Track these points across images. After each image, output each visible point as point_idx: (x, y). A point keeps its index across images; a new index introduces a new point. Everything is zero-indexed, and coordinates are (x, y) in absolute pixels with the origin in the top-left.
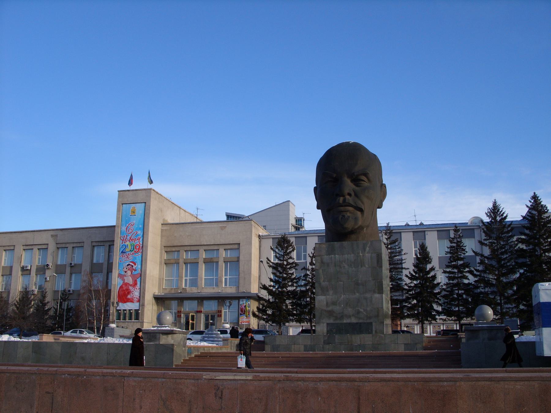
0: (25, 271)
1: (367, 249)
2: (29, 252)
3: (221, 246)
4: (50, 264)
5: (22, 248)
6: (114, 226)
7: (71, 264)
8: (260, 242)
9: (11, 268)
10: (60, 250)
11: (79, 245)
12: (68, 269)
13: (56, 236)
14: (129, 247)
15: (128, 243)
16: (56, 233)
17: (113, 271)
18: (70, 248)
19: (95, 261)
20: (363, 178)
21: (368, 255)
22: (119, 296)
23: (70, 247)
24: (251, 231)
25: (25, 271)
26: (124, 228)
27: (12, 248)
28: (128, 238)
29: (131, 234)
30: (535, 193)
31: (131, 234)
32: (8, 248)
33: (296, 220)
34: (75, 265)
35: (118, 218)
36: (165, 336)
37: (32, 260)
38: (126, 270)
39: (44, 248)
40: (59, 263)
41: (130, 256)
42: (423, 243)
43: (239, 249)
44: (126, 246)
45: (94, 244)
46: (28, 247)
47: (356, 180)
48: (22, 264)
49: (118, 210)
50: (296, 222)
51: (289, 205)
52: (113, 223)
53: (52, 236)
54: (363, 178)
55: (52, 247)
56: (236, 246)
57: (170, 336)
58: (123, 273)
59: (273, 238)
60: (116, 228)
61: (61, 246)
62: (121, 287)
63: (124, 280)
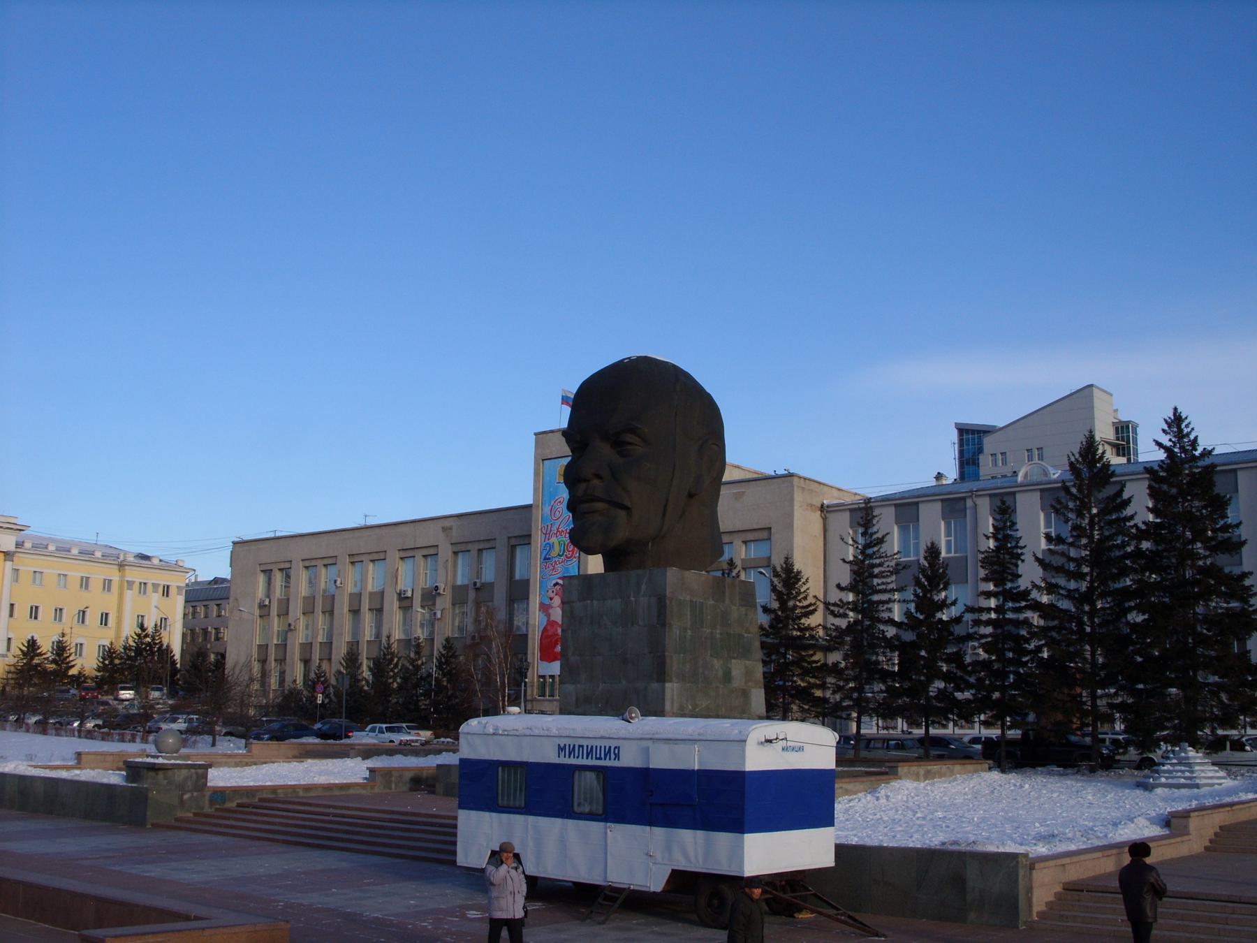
0: (405, 601)
1: (644, 587)
2: (410, 562)
3: (736, 535)
4: (442, 586)
5: (398, 555)
6: (529, 506)
7: (475, 584)
8: (825, 519)
9: (382, 593)
10: (460, 555)
11: (487, 545)
12: (472, 594)
13: (451, 528)
14: (557, 548)
15: (554, 540)
16: (445, 523)
17: (531, 596)
18: (474, 553)
19: (517, 577)
20: (629, 438)
21: (644, 600)
22: (542, 649)
23: (474, 548)
24: (792, 500)
25: (405, 601)
26: (547, 510)
27: (432, 551)
28: (555, 528)
29: (558, 522)
30: (1176, 409)
31: (558, 522)
32: (375, 557)
33: (1117, 429)
34: (483, 585)
35: (536, 490)
36: (152, 774)
37: (410, 577)
38: (552, 595)
39: (430, 553)
40: (459, 582)
41: (559, 566)
42: (933, 544)
43: (769, 539)
44: (551, 546)
45: (513, 542)
46: (407, 553)
47: (618, 444)
48: (400, 586)
49: (536, 474)
50: (1117, 432)
51: (1091, 396)
52: (528, 500)
53: (444, 529)
54: (629, 438)
55: (445, 552)
56: (765, 534)
57: (161, 774)
58: (547, 602)
59: (851, 510)
60: (534, 511)
61: (459, 549)
62: (545, 630)
63: (548, 615)
